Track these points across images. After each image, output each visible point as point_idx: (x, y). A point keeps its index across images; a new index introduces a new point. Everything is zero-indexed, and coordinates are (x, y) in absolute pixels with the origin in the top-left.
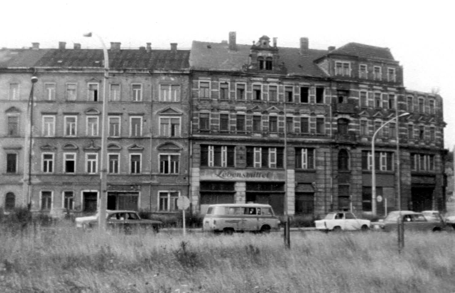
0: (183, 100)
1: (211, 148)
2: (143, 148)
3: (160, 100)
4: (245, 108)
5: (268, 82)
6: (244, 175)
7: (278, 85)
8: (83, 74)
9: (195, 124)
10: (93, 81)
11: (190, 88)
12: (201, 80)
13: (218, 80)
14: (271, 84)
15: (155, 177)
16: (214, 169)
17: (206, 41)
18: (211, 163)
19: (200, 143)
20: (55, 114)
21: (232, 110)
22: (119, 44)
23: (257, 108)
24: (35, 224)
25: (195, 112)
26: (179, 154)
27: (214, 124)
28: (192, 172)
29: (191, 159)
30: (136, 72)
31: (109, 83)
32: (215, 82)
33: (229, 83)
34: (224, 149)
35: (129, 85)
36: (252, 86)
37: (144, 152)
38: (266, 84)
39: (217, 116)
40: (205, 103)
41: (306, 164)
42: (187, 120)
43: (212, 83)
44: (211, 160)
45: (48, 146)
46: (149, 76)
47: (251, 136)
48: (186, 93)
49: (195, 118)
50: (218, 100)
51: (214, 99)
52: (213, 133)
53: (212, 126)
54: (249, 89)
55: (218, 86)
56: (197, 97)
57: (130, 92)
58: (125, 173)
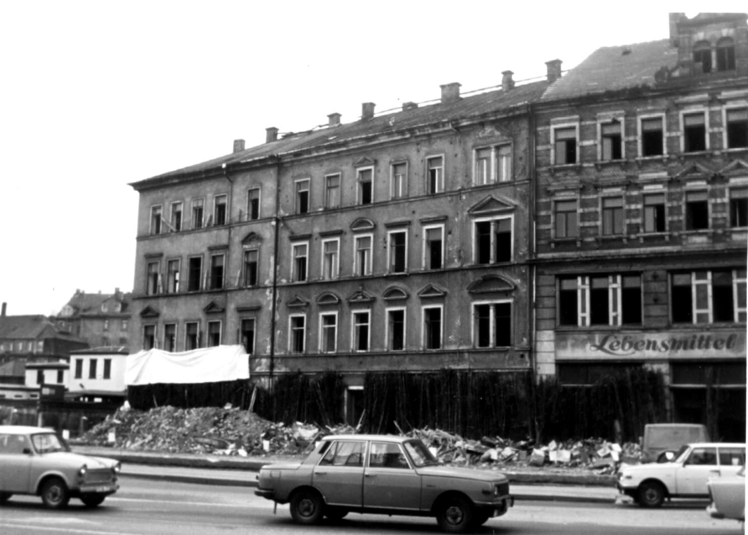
1: (583, 283)
2: (445, 293)
4: (664, 174)
5: (723, 102)
6: (664, 345)
7: (706, 110)
8: (349, 153)
9: (543, 227)
10: (366, 162)
11: (530, 147)
12: (555, 123)
14: (731, 105)
15: (466, 355)
18: (584, 319)
19: (556, 272)
21: (630, 184)
23: (695, 169)
24: (442, 454)
27: (587, 224)
28: (536, 341)
30: (430, 131)
31: (390, 162)
32: (588, 123)
33: (622, 119)
34: (615, 281)
36: (681, 117)
37: (446, 299)
38: (716, 108)
39: (594, 203)
40: (566, 175)
41: (587, 315)
42: (524, 223)
45: (298, 301)
46: (456, 135)
47: (680, 244)
48: (524, 160)
49: (543, 213)
50: (596, 165)
51: (585, 165)
52: (585, 246)
53: (582, 228)
54: (674, 127)
55: (595, 133)
56: (549, 164)
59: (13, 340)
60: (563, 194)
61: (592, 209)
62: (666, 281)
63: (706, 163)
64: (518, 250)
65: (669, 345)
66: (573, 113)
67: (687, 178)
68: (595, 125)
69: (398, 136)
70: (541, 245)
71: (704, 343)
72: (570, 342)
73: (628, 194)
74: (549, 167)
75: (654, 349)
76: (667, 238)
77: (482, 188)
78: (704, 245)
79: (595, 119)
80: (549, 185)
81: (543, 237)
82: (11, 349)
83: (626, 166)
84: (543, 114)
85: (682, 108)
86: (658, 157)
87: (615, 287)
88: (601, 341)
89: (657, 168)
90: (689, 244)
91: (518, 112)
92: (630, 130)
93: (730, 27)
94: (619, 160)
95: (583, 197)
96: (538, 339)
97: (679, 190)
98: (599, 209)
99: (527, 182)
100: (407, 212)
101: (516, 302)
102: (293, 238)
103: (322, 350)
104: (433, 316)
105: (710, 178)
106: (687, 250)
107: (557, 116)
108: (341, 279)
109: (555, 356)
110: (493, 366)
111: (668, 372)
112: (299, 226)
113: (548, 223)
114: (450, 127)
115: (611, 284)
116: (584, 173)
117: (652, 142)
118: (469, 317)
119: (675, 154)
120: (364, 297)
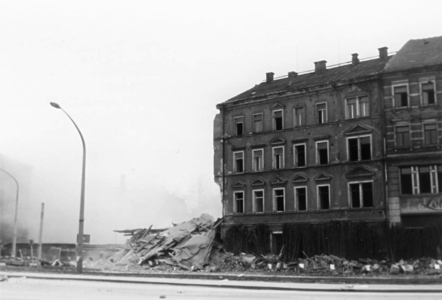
0: (372, 114)
1: (415, 170)
2: (331, 178)
3: (347, 117)
8: (267, 102)
9: (390, 141)
12: (394, 84)
13: (417, 81)
15: (346, 212)
16: (420, 197)
17: (421, 38)
18: (416, 190)
20: (244, 148)
22: (324, 62)
25: (389, 126)
26: (372, 181)
27: (416, 139)
29: (387, 187)
30: (318, 89)
32: (414, 83)
35: (313, 106)
37: (332, 181)
40: (402, 113)
43: (410, 86)
44: (416, 185)
45: (239, 184)
50: (420, 107)
51: (413, 107)
52: (415, 151)
53: (413, 141)
56: (391, 107)
57: (315, 114)
58: (313, 209)
60: (401, 123)
69: (298, 92)
72: (408, 204)
73: (439, 122)
77: (355, 120)
91: (372, 78)
101: (375, 181)
102: (234, 149)
104: (324, 190)
120: (280, 181)
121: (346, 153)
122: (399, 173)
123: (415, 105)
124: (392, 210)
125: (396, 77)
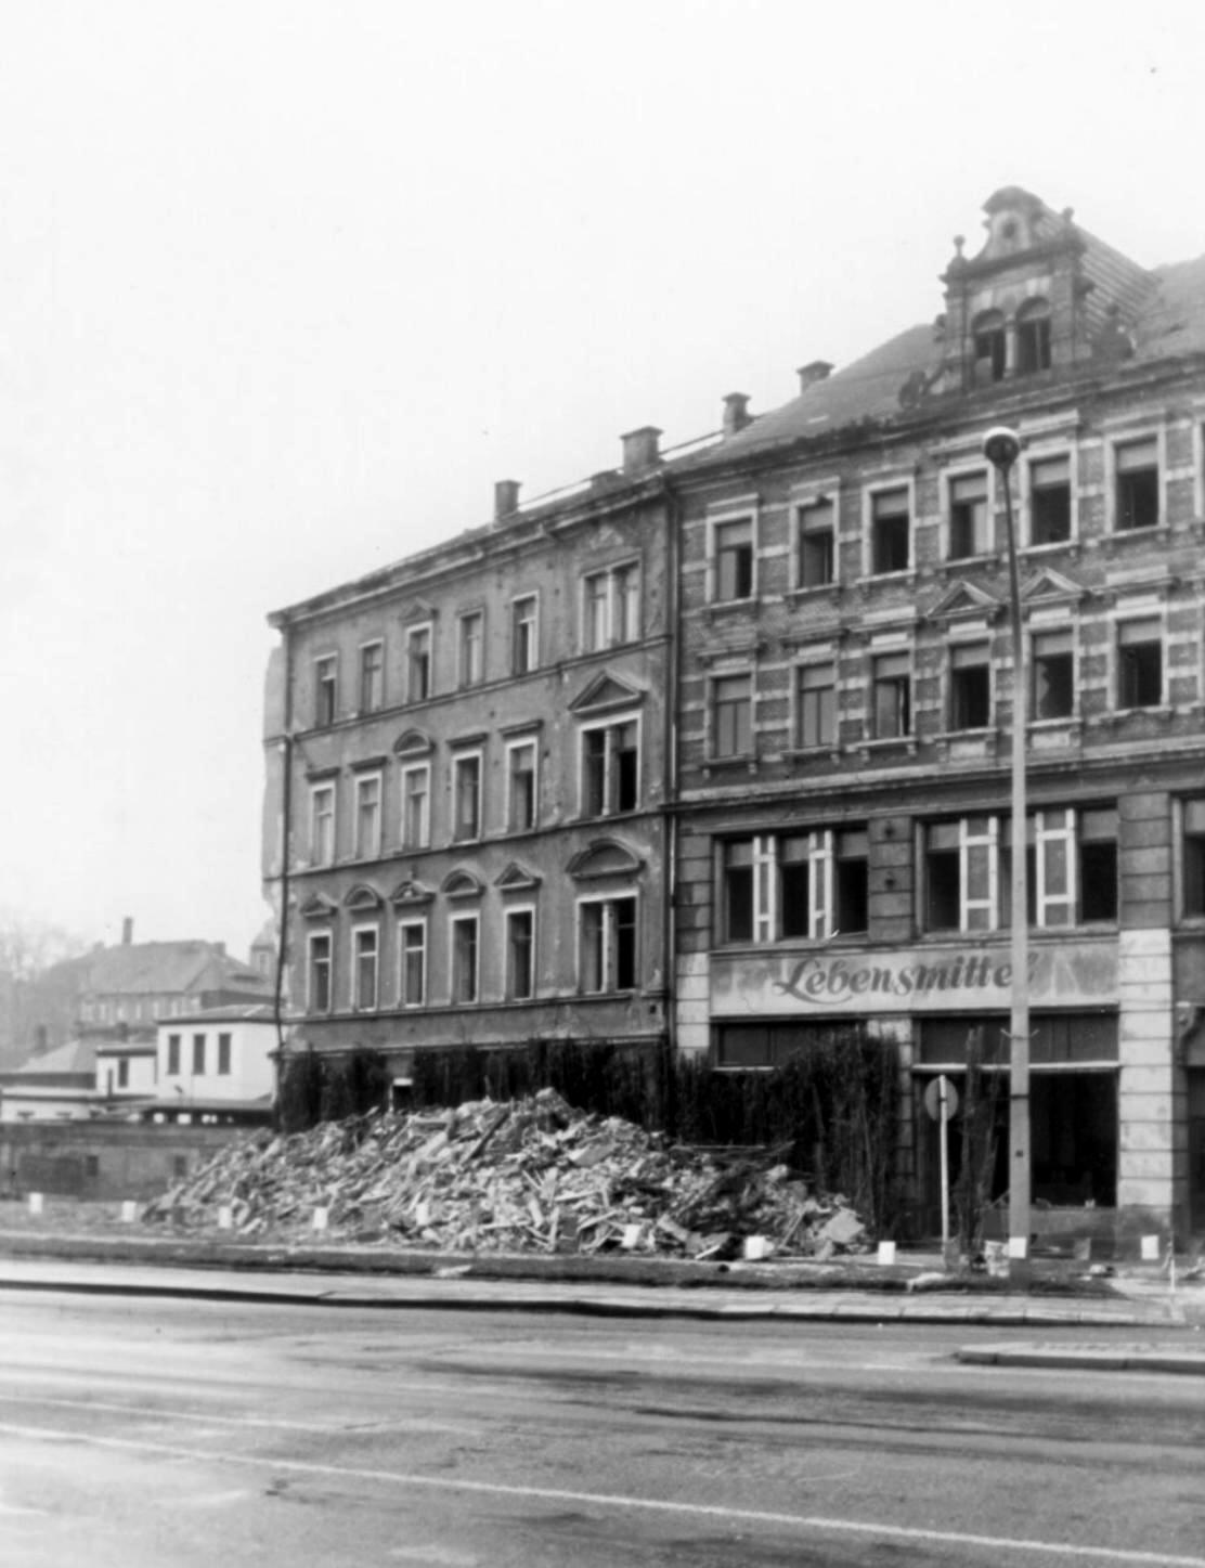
1: (764, 850)
6: (904, 980)
9: (690, 736)
22: (650, 434)
23: (964, 598)
27: (770, 726)
33: (834, 495)
34: (820, 845)
36: (943, 484)
37: (542, 893)
38: (1090, 443)
40: (733, 624)
50: (787, 598)
51: (768, 599)
52: (764, 771)
53: (760, 734)
56: (701, 602)
59: (152, 995)
60: (727, 663)
61: (777, 694)
62: (912, 840)
63: (985, 581)
64: (650, 790)
65: (913, 980)
66: (747, 489)
67: (948, 616)
68: (786, 511)
69: (464, 556)
70: (688, 773)
71: (977, 973)
72: (736, 977)
73: (844, 656)
74: (702, 608)
75: (886, 988)
76: (912, 750)
77: (592, 658)
78: (979, 761)
79: (786, 499)
80: (702, 645)
81: (690, 757)
82: (138, 1015)
83: (841, 596)
84: (694, 495)
85: (945, 465)
86: (897, 574)
87: (819, 855)
88: (792, 970)
89: (897, 599)
90: (954, 759)
91: (645, 495)
92: (851, 518)
93: (1041, 274)
94: (826, 586)
95: (765, 667)
96: (680, 971)
97: (934, 643)
98: (791, 693)
99: (662, 641)
100: (484, 714)
101: (642, 893)
102: (314, 778)
103: (358, 1005)
104: (521, 922)
105: (992, 615)
106: (948, 772)
107: (718, 499)
108: (384, 858)
109: (710, 1008)
110: (602, 1032)
111: (909, 1039)
112: (321, 751)
113: (699, 726)
114: (540, 533)
115: (813, 850)
116: (764, 617)
117: (891, 539)
118: (572, 928)
119: (931, 564)
120: (415, 893)
121: (574, 784)
122: (1177, 822)
123: (772, 592)
124: (682, 1000)
125: (714, 486)
